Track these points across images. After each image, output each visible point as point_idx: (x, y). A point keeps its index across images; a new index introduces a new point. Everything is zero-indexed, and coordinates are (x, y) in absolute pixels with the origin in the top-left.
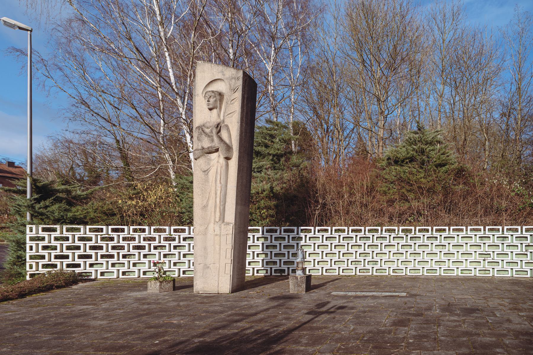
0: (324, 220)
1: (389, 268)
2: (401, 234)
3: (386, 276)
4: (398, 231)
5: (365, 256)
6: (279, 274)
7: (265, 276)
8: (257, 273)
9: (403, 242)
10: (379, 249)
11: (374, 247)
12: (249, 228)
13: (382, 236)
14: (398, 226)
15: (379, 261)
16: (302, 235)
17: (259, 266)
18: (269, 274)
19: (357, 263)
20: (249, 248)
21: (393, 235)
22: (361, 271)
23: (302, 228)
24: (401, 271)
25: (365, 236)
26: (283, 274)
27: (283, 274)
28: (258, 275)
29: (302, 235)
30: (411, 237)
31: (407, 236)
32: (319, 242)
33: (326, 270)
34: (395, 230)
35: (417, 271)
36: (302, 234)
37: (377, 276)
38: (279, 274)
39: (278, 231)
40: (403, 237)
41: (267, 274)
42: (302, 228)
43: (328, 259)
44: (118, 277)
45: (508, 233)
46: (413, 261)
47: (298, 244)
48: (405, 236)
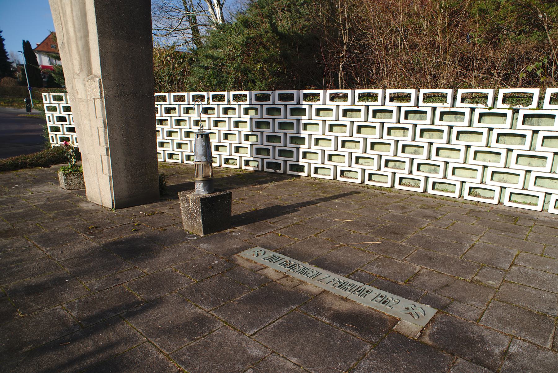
0: (360, 74)
1: (463, 182)
2: (501, 107)
3: (454, 200)
4: (495, 98)
5: (415, 153)
6: (272, 171)
7: (256, 171)
8: (370, 179)
9: (503, 126)
10: (445, 140)
11: (435, 133)
12: (156, 94)
13: (453, 110)
14: (455, 88)
15: (442, 165)
16: (305, 105)
17: (246, 154)
18: (260, 169)
19: (397, 163)
20: (305, 129)
21: (480, 108)
22: (514, 197)
23: (305, 91)
24: (490, 194)
25: (416, 109)
26: (278, 171)
27: (278, 171)
28: (370, 183)
29: (305, 105)
30: (526, 116)
31: (516, 111)
32: (391, 121)
33: (434, 183)
34: (485, 97)
35: (529, 200)
36: (304, 103)
37: (434, 197)
38: (272, 171)
39: (271, 98)
40: (505, 115)
41: (257, 169)
42: (305, 91)
43: (439, 161)
44: (335, 179)
45: (235, 103)
46: (522, 174)
47: (298, 120)
48: (510, 113)
